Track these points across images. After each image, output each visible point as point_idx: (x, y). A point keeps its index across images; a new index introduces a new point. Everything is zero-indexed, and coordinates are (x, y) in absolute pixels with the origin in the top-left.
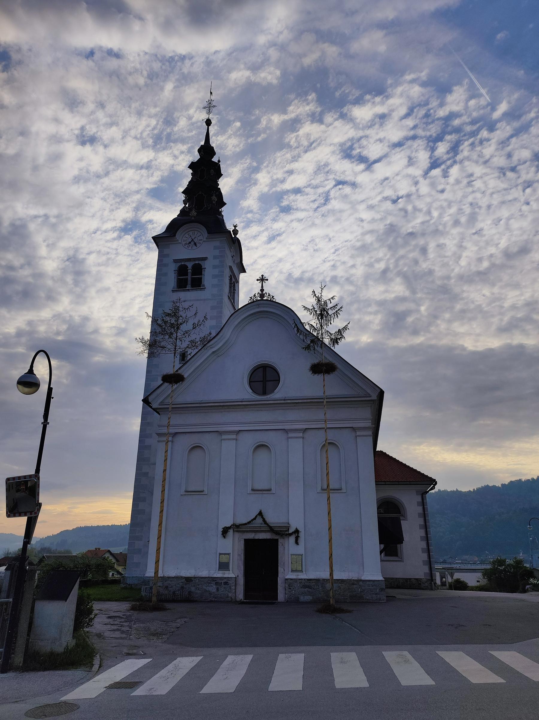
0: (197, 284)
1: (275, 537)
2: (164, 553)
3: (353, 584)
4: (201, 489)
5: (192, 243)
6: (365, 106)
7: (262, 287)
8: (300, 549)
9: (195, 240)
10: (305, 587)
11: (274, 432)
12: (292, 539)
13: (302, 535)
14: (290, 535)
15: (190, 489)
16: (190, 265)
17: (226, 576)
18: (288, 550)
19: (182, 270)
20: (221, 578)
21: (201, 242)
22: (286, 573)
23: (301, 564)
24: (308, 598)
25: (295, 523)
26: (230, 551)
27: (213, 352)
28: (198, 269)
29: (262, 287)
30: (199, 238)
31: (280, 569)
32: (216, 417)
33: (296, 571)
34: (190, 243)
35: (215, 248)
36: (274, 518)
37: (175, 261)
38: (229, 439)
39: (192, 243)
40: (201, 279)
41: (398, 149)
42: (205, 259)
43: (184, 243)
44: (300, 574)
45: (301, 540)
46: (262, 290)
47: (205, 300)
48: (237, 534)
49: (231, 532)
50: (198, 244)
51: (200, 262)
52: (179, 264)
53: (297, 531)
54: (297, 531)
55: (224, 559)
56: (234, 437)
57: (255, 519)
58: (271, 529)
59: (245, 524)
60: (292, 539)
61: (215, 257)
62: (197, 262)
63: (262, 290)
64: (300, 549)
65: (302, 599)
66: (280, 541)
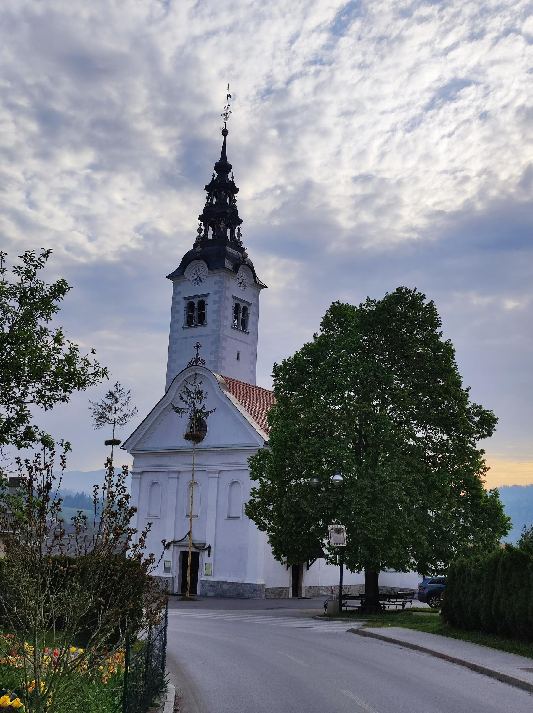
0: (201, 320)
1: (198, 551)
2: (215, 552)
3: (239, 586)
4: (156, 514)
5: (198, 279)
6: (429, 22)
7: (197, 352)
8: (210, 560)
9: (200, 277)
10: (211, 586)
11: (202, 473)
12: (206, 552)
13: (212, 550)
14: (206, 549)
15: (152, 514)
16: (196, 301)
17: (167, 576)
18: (204, 560)
19: (190, 307)
20: (164, 578)
21: (205, 277)
22: (202, 577)
23: (214, 570)
24: (212, 594)
25: (210, 542)
26: (171, 559)
27: (165, 409)
28: (202, 305)
29: (197, 352)
30: (204, 274)
31: (199, 573)
32: (166, 460)
33: (207, 575)
34: (196, 279)
35: (216, 283)
36: (197, 538)
37: (185, 299)
38: (173, 478)
39: (198, 279)
40: (204, 313)
41: (462, 75)
42: (207, 295)
43: (192, 279)
44: (209, 577)
45: (212, 554)
46: (197, 355)
47: (207, 335)
48: (176, 548)
49: (172, 545)
50: (202, 280)
51: (204, 299)
52: (188, 301)
53: (209, 548)
54: (209, 548)
55: (167, 565)
56: (176, 476)
57: (185, 537)
58: (194, 545)
59: (179, 541)
60: (206, 552)
61: (216, 293)
62: (201, 299)
63: (197, 355)
64: (210, 560)
65: (209, 594)
66: (201, 554)
